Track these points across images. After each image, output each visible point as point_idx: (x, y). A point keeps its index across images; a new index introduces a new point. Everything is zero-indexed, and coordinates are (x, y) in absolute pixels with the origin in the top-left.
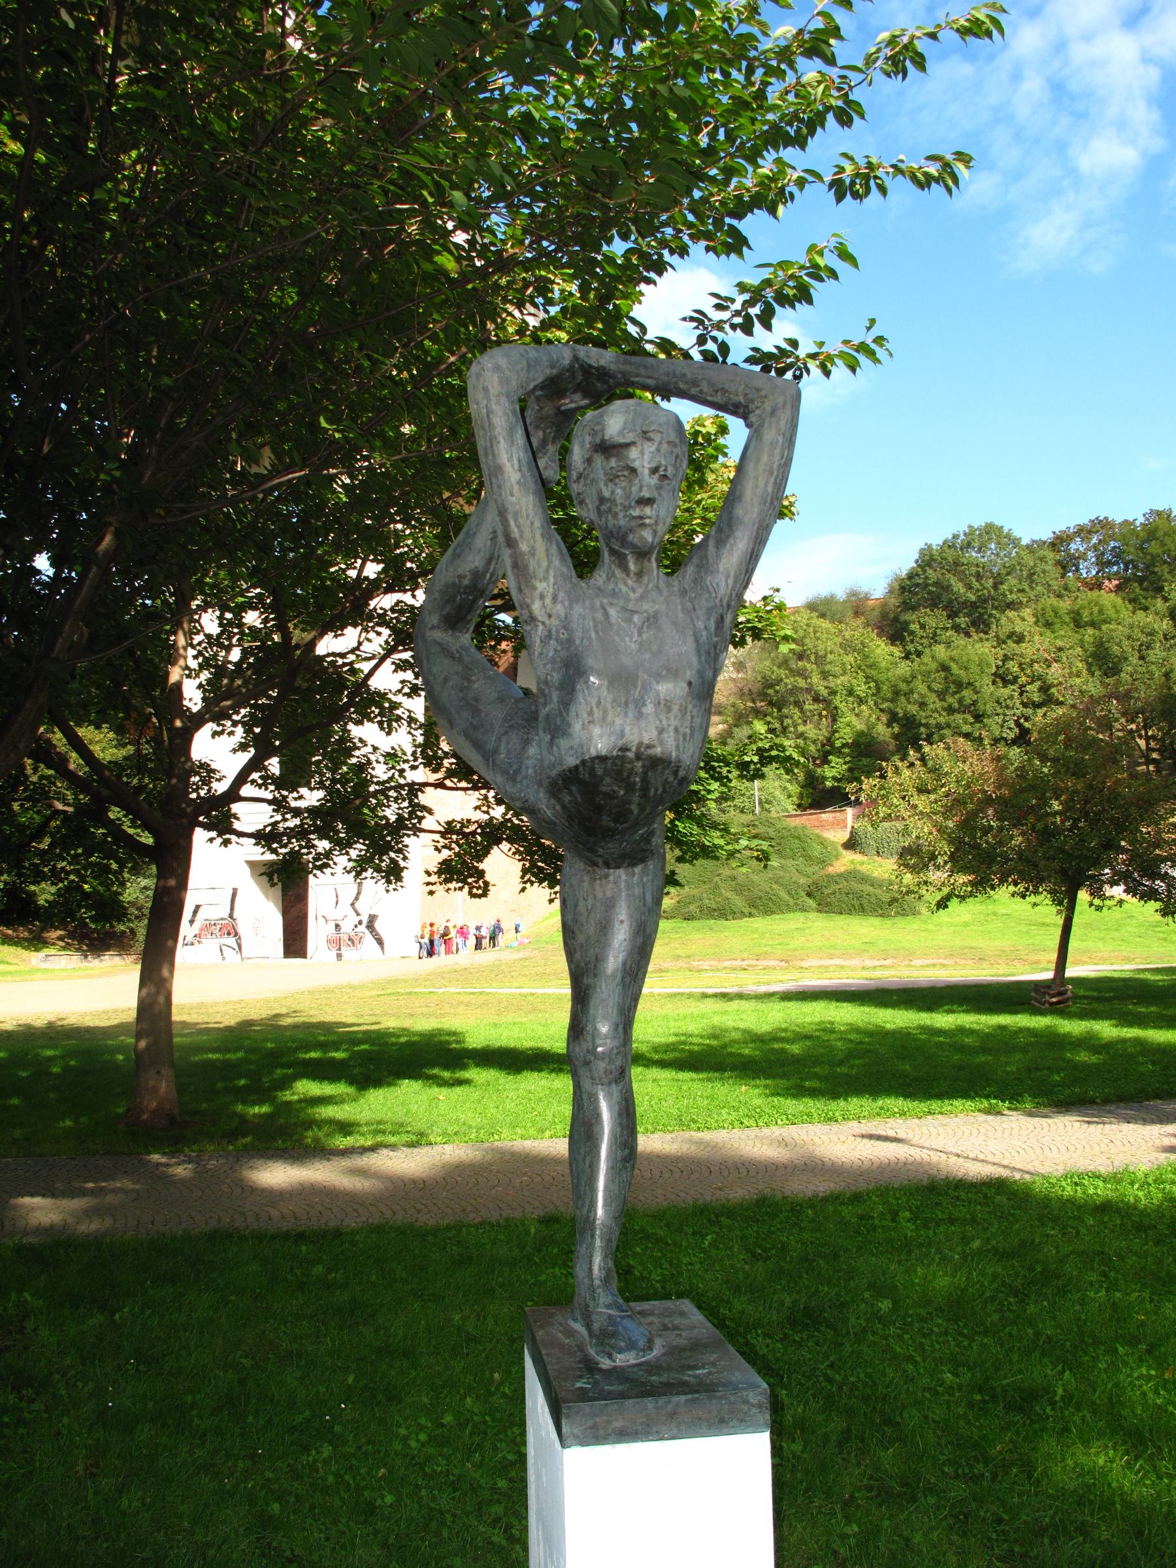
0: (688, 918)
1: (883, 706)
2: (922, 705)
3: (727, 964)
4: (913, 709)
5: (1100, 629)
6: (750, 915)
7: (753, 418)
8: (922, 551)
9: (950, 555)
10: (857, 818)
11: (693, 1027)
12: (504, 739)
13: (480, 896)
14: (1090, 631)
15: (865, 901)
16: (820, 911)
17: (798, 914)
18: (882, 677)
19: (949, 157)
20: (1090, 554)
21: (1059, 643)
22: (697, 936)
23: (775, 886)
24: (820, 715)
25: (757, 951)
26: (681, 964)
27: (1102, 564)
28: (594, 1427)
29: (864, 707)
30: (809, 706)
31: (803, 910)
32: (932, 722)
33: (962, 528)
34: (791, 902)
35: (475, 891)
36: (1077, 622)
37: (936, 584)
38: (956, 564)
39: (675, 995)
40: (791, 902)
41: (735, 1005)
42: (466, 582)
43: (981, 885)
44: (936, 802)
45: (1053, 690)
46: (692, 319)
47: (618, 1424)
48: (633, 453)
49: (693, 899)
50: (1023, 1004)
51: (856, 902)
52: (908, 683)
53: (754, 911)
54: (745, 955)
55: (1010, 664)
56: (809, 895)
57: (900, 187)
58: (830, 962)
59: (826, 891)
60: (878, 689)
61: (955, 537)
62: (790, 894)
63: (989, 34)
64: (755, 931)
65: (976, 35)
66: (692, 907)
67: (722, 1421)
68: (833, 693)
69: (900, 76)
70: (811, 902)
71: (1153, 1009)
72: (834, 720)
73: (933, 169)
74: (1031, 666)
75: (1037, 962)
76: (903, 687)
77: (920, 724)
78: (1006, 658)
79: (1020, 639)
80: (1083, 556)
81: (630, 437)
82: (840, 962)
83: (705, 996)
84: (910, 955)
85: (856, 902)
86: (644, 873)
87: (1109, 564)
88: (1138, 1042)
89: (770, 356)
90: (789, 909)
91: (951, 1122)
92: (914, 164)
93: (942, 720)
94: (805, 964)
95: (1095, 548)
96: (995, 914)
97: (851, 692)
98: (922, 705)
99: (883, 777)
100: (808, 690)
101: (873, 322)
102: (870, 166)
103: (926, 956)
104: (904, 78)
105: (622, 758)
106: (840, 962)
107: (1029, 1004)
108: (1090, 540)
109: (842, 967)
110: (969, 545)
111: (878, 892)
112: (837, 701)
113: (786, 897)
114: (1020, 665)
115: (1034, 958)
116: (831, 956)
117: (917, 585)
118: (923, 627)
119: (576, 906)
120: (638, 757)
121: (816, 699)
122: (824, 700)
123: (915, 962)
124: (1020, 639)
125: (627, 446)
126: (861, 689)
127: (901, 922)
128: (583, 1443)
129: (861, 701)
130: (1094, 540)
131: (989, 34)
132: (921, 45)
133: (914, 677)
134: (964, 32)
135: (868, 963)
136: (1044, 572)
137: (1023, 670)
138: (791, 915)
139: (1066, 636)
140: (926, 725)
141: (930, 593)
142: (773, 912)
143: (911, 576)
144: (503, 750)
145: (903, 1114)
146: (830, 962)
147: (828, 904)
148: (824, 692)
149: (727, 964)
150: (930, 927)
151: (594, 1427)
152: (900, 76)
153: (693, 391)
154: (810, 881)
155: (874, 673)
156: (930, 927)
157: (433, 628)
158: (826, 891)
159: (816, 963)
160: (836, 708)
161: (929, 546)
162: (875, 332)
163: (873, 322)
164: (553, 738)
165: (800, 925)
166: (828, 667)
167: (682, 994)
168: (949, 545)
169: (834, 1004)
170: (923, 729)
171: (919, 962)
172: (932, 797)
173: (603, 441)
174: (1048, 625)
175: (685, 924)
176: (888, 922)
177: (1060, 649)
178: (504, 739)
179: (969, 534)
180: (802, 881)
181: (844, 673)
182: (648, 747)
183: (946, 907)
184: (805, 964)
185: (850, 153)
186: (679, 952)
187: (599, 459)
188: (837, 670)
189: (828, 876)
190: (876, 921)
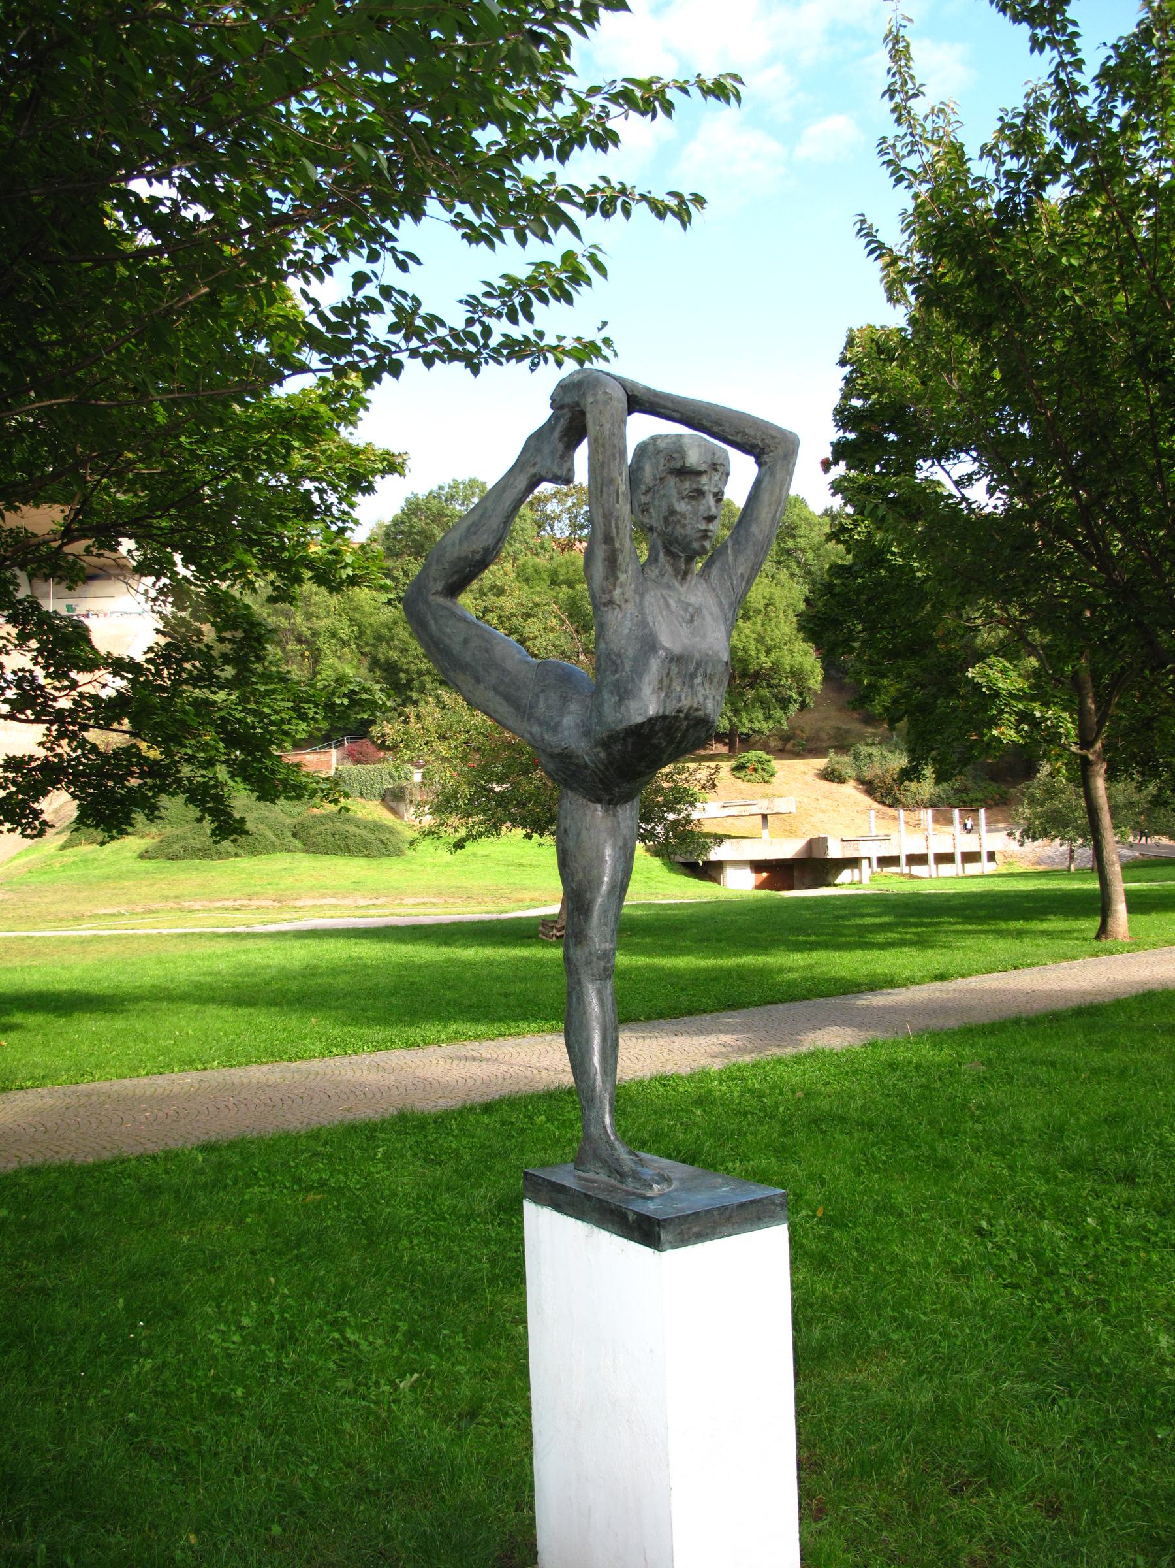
0: (173, 858)
1: (366, 650)
2: (404, 651)
3: (219, 904)
4: (394, 655)
5: (573, 588)
6: (236, 855)
7: (766, 458)
8: (407, 501)
9: (435, 505)
10: (340, 761)
11: (223, 965)
12: (542, 696)
13: (32, 837)
14: (564, 589)
15: (350, 842)
16: (306, 851)
17: (284, 855)
18: (366, 621)
19: (687, 197)
20: (565, 516)
21: (536, 599)
22: (184, 876)
23: (261, 826)
24: (302, 655)
25: (247, 890)
26: (171, 904)
27: (575, 526)
28: (681, 1233)
29: (346, 650)
30: (292, 647)
31: (290, 850)
32: (412, 667)
33: (447, 481)
34: (278, 842)
35: (29, 831)
36: (554, 582)
37: (420, 533)
38: (441, 515)
39: (185, 935)
40: (278, 842)
41: (250, 944)
42: (478, 557)
43: (493, 827)
44: (456, 748)
45: (529, 643)
46: (467, 303)
47: (695, 1230)
48: (704, 479)
49: (177, 839)
50: (530, 937)
51: (341, 842)
52: (390, 629)
53: (240, 851)
54: (237, 895)
55: (490, 616)
56: (294, 835)
57: (641, 210)
58: (323, 902)
59: (312, 832)
60: (361, 633)
61: (440, 488)
62: (275, 834)
63: (728, 101)
64: (243, 871)
65: (717, 97)
66: (176, 847)
67: (759, 1219)
68: (316, 634)
69: (650, 116)
70: (297, 843)
71: (648, 940)
72: (316, 662)
73: (673, 203)
74: (509, 619)
75: (521, 900)
76: (385, 632)
77: (402, 670)
78: (486, 610)
79: (500, 592)
80: (557, 518)
81: (703, 467)
82: (333, 901)
83: (217, 936)
84: (400, 894)
85: (341, 842)
86: (632, 808)
87: (582, 527)
88: (652, 969)
89: (517, 342)
90: (275, 849)
91: (528, 1040)
92: (659, 194)
93: (423, 667)
94: (298, 903)
95: (569, 510)
96: (474, 855)
97: (334, 635)
98: (404, 651)
99: (406, 722)
100: (292, 631)
101: (605, 324)
102: (623, 191)
103: (416, 895)
104: (654, 118)
105: (676, 718)
106: (333, 901)
107: (536, 937)
108: (565, 502)
109: (335, 906)
110: (452, 497)
111: (364, 833)
112: (320, 642)
113: (272, 837)
114: (500, 617)
115: (519, 896)
116: (324, 896)
117: (402, 532)
118: (406, 574)
119: (578, 835)
120: (686, 717)
121: (299, 640)
122: (307, 641)
123: (406, 901)
124: (500, 592)
125: (699, 473)
126: (345, 633)
127: (386, 862)
128: (674, 1247)
129: (344, 644)
130: (569, 503)
131: (728, 101)
132: (672, 94)
133: (395, 623)
134: (706, 92)
135: (361, 902)
136: (523, 530)
137: (501, 622)
138: (278, 855)
139: (542, 594)
140: (407, 671)
141: (414, 540)
142: (259, 853)
143: (396, 523)
144: (541, 705)
145: (477, 1037)
146: (323, 902)
147: (314, 845)
148: (308, 633)
149: (219, 904)
150: (414, 867)
151: (681, 1233)
152: (650, 116)
153: (716, 429)
154: (295, 821)
155: (357, 616)
156: (414, 867)
157: (436, 593)
158: (312, 832)
159: (310, 902)
160: (318, 650)
161: (416, 496)
162: (605, 333)
163: (605, 324)
164: (621, 699)
165: (286, 865)
166: (311, 609)
167: (193, 934)
168: (433, 496)
169: (353, 941)
170: (402, 675)
171: (411, 901)
172: (453, 743)
173: (683, 467)
174: (527, 580)
175: (168, 864)
176: (374, 863)
177: (537, 605)
178: (542, 696)
179: (455, 486)
180: (288, 821)
181: (328, 615)
182: (697, 710)
183: (463, 847)
184: (298, 903)
185: (609, 176)
186: (166, 893)
187: (672, 481)
188: (321, 612)
189: (314, 816)
190: (362, 862)
